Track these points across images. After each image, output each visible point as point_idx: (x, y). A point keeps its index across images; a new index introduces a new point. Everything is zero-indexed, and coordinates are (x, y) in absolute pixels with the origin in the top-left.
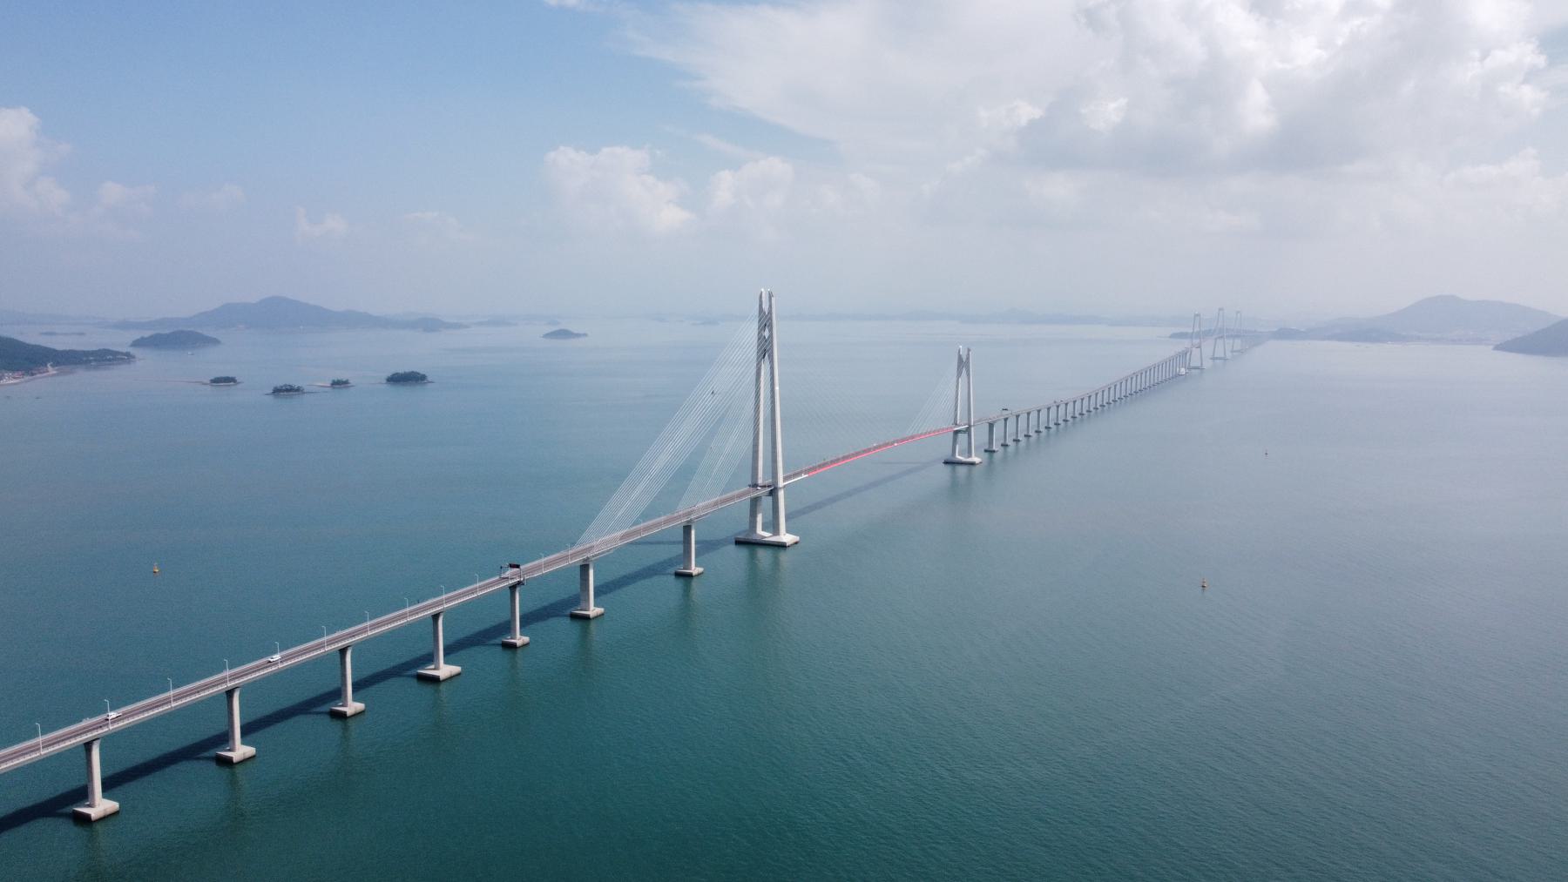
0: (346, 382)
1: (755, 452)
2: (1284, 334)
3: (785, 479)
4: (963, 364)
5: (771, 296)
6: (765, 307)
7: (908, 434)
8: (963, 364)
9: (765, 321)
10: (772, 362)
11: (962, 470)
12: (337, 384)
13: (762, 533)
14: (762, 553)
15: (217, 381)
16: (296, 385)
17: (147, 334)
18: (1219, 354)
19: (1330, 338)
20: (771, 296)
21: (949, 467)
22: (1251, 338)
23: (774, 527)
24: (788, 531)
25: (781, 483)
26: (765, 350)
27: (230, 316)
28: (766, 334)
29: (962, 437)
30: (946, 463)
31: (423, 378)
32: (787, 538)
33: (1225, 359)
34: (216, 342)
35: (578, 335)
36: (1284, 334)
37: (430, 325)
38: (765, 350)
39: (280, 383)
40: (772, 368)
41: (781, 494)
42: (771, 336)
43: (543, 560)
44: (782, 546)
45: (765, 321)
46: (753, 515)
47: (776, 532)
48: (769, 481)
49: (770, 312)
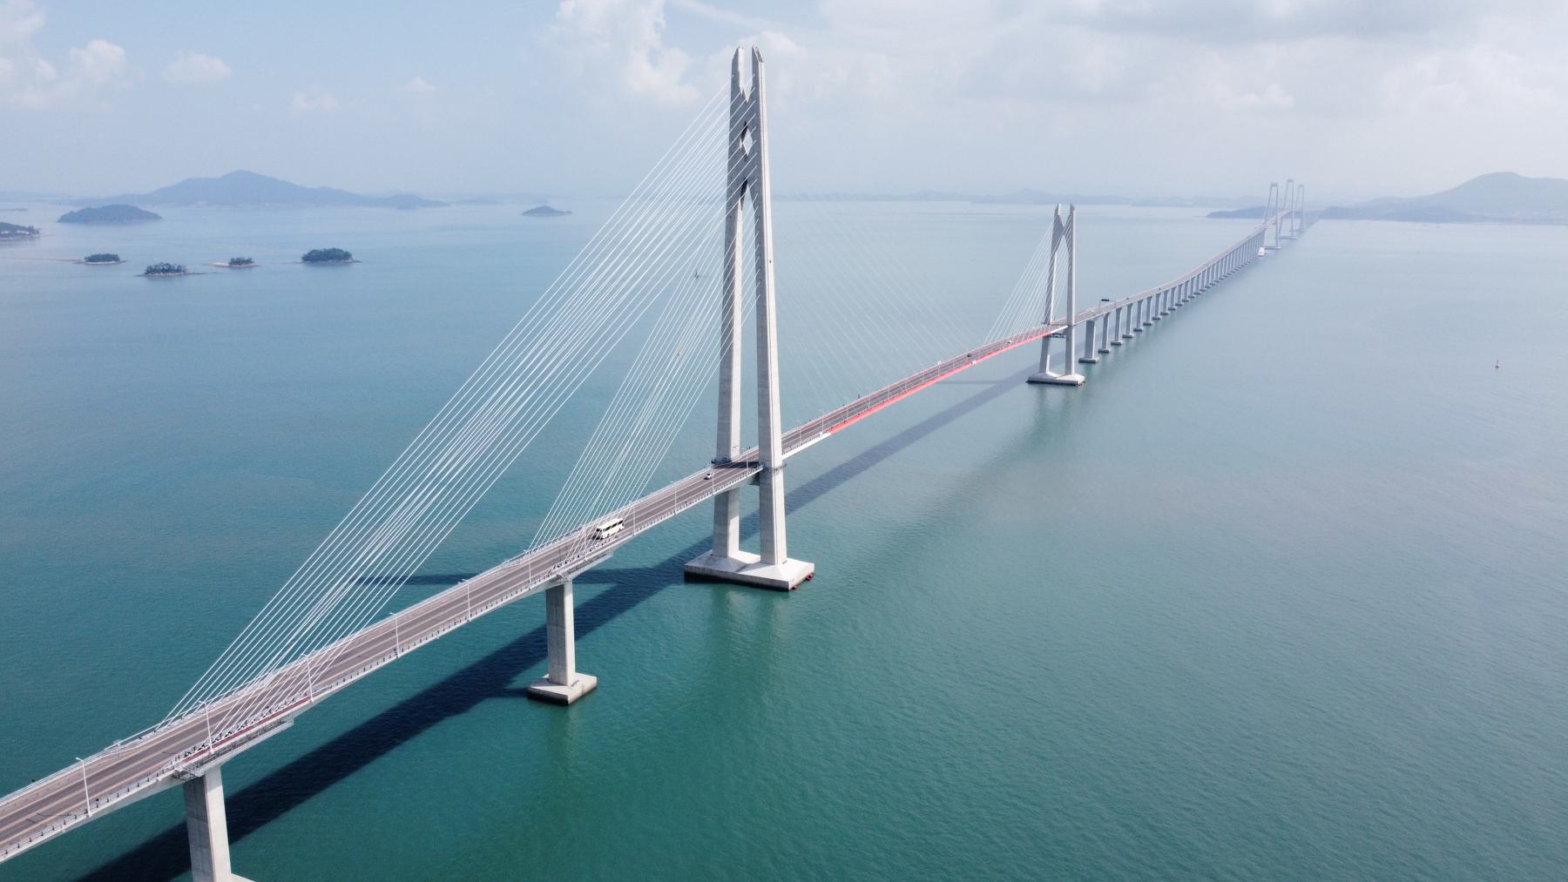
0: (249, 261)
1: (725, 394)
2: (1336, 213)
3: (788, 443)
4: (1061, 230)
5: (756, 60)
6: (745, 85)
7: (988, 342)
8: (1061, 230)
9: (745, 117)
10: (758, 204)
11: (1054, 394)
12: (237, 263)
13: (739, 556)
14: (739, 600)
15: (94, 259)
16: (174, 261)
17: (76, 210)
18: (1285, 233)
19: (1387, 217)
20: (756, 60)
21: (1034, 389)
22: (1305, 216)
23: (758, 530)
24: (792, 554)
25: (778, 458)
26: (744, 179)
27: (191, 194)
28: (747, 143)
29: (1057, 345)
30: (1031, 382)
31: (347, 256)
32: (789, 570)
33: (1291, 239)
34: (156, 217)
35: (561, 213)
36: (1336, 213)
37: (406, 202)
38: (744, 179)
39: (156, 261)
40: (759, 217)
41: (778, 481)
42: (757, 147)
43: (82, 767)
44: (778, 588)
45: (745, 117)
46: (721, 519)
47: (768, 557)
48: (753, 452)
49: (755, 96)
